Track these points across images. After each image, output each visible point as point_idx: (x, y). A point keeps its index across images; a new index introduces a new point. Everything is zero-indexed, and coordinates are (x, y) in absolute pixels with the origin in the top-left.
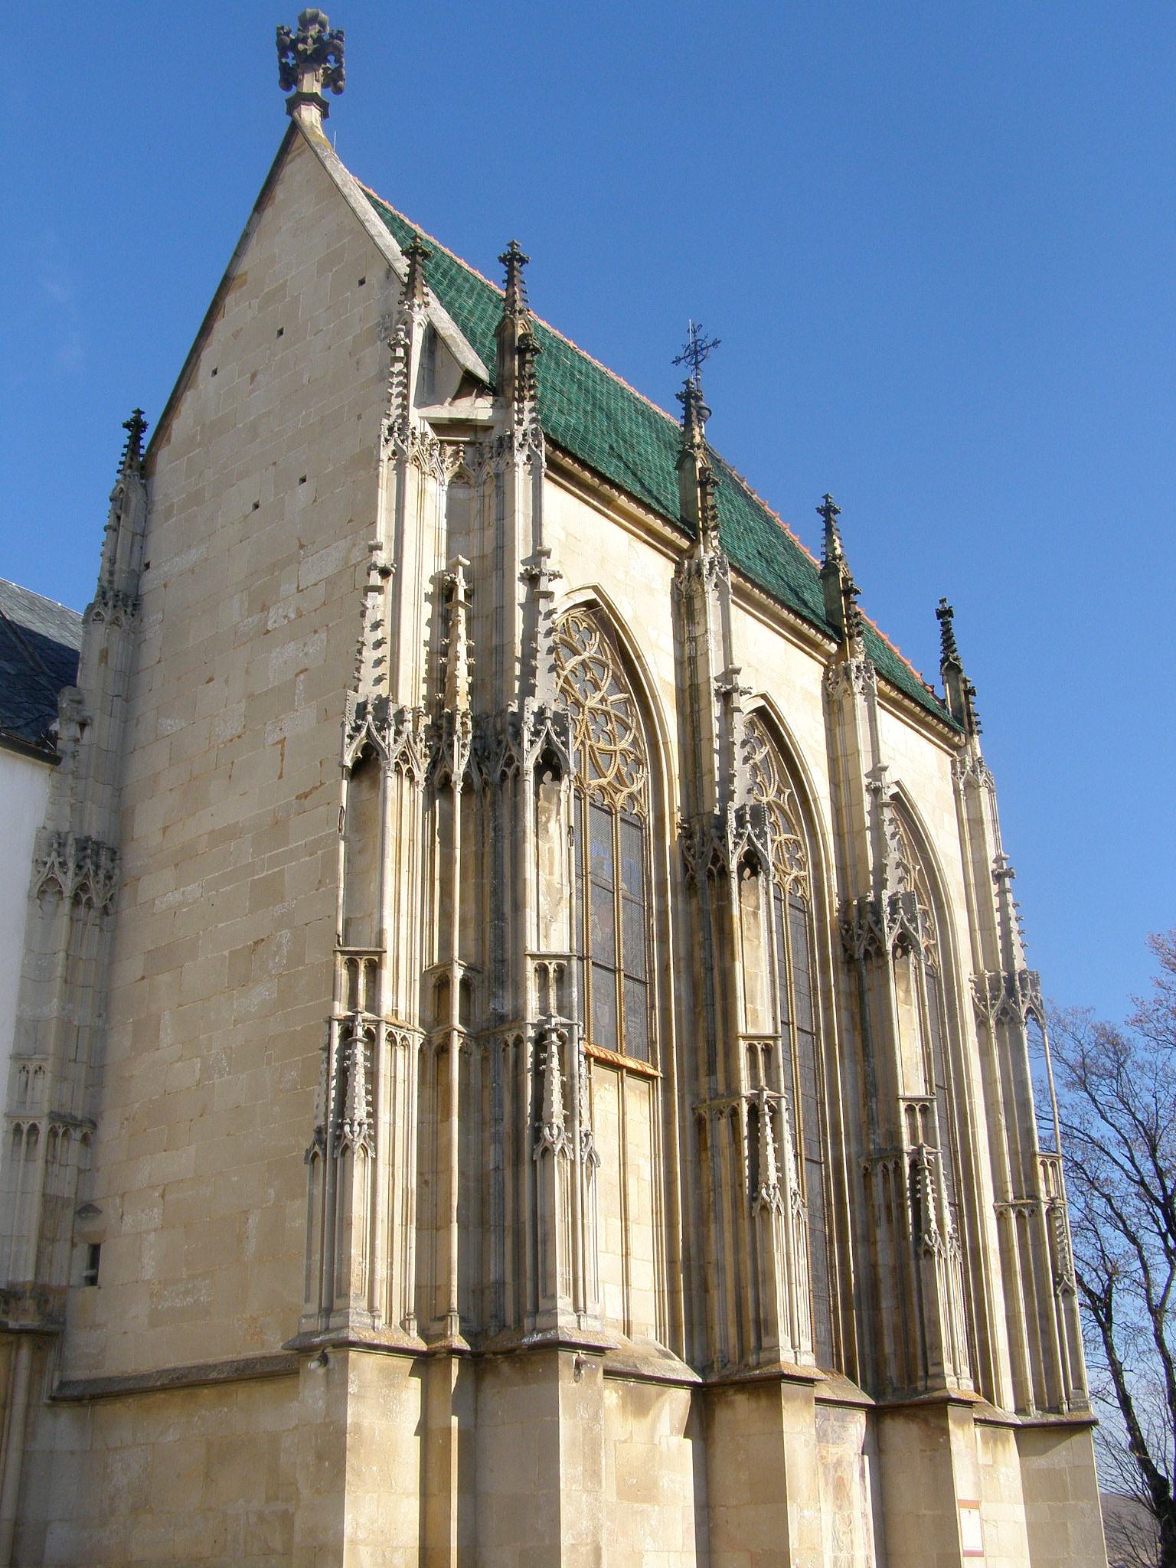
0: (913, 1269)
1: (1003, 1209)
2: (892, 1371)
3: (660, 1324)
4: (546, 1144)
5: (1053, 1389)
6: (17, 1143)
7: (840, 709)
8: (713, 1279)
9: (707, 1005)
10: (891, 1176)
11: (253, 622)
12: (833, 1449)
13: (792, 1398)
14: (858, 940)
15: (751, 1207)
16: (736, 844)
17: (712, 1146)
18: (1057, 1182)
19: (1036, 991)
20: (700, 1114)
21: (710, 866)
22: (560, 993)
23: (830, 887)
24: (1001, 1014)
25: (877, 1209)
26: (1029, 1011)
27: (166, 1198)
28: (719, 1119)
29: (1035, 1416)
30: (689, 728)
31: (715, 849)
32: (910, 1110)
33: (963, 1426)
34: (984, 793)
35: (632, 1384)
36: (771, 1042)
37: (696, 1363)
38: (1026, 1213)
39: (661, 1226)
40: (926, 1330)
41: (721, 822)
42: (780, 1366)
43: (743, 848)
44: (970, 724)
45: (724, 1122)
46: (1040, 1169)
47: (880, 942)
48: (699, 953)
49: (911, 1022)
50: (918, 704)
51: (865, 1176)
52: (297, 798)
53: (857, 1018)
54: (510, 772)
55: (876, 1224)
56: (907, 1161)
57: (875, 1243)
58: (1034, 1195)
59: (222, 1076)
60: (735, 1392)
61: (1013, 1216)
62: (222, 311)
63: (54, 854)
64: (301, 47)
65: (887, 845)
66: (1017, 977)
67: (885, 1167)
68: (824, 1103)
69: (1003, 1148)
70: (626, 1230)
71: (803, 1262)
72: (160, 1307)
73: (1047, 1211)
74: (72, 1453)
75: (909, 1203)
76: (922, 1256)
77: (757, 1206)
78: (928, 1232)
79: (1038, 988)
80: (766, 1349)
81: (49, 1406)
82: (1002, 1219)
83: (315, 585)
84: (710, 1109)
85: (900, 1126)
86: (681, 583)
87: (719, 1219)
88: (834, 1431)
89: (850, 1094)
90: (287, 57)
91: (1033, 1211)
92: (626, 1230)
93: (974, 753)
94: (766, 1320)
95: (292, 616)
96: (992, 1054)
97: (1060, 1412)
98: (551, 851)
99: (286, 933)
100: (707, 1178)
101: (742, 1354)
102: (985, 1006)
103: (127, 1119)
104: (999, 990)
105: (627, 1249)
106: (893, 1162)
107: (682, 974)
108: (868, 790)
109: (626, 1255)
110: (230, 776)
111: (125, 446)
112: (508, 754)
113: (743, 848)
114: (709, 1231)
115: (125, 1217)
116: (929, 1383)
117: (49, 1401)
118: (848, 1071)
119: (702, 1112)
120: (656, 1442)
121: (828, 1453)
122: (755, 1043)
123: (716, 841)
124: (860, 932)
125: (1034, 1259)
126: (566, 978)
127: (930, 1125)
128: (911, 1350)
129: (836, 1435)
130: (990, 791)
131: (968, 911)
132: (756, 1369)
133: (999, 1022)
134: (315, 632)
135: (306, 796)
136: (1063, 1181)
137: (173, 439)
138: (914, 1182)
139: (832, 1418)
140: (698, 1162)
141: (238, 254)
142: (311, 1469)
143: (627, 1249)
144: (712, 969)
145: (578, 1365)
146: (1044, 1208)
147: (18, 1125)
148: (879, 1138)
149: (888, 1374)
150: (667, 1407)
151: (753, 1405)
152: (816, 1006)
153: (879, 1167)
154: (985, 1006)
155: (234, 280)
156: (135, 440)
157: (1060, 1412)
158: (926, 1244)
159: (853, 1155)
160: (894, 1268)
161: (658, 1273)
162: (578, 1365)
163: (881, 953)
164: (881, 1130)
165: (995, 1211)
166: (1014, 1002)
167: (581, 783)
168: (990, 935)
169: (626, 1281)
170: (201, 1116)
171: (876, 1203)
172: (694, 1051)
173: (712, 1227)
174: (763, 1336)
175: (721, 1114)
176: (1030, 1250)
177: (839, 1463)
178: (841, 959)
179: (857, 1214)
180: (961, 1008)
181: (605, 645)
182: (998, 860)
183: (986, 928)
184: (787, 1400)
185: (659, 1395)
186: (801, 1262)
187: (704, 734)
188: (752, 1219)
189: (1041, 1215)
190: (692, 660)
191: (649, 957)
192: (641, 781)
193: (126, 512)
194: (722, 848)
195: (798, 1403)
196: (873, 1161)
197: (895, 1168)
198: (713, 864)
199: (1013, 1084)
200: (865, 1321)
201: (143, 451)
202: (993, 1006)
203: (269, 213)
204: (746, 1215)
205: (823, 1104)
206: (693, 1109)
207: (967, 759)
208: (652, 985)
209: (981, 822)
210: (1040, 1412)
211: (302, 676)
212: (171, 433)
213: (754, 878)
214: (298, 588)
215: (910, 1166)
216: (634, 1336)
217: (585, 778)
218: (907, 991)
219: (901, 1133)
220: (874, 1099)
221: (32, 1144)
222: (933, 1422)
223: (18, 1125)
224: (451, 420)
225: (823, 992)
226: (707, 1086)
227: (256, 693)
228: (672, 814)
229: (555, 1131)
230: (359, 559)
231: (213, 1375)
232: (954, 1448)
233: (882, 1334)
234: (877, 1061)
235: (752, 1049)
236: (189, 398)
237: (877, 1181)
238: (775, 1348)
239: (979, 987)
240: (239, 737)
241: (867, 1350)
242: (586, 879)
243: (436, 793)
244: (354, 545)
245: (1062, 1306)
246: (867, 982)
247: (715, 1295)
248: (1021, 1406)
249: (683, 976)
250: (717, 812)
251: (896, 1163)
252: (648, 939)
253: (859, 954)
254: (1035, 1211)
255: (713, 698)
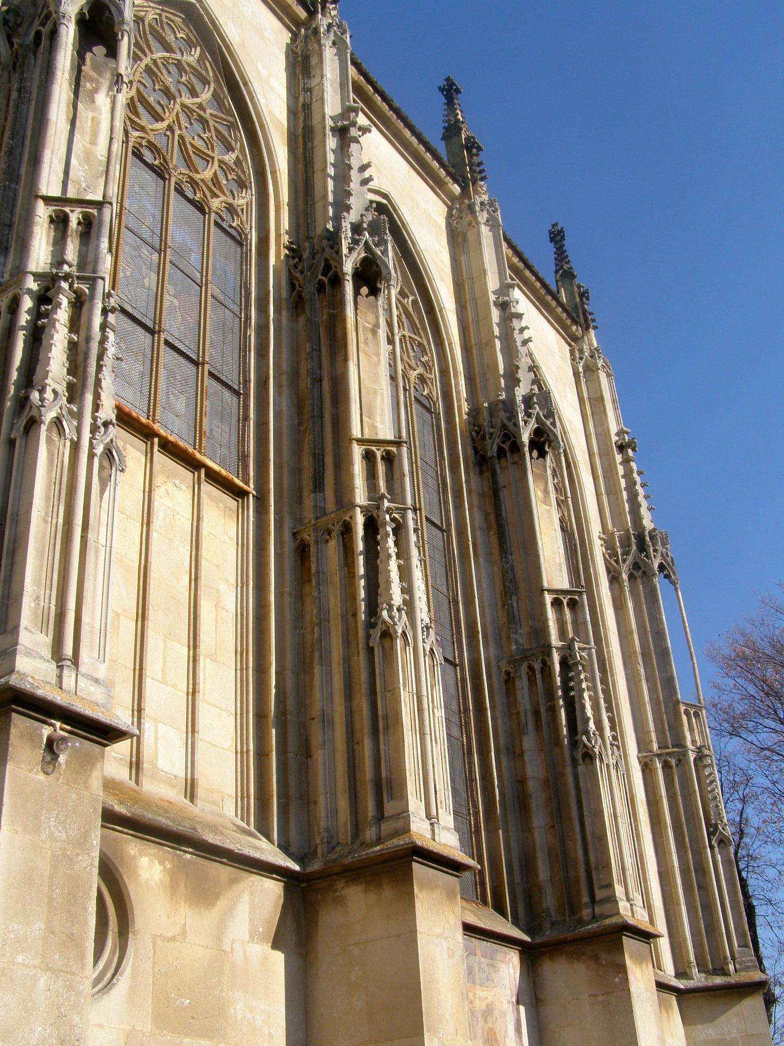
0: (570, 778)
1: (647, 760)
2: (549, 901)
3: (243, 795)
4: (34, 413)
5: (716, 948)
7: (465, 239)
8: (317, 734)
9: (313, 417)
10: (539, 676)
12: (481, 992)
13: (430, 886)
14: (490, 438)
15: (368, 637)
16: (351, 250)
17: (318, 572)
18: (702, 732)
19: (666, 549)
20: (302, 541)
21: (320, 277)
22: (84, 248)
23: (458, 393)
24: (634, 568)
25: (522, 717)
26: (662, 567)
28: (327, 541)
29: (698, 979)
30: (301, 166)
31: (326, 260)
32: (557, 603)
33: (640, 964)
34: (602, 376)
35: (188, 856)
36: (394, 449)
37: (292, 849)
38: (673, 762)
39: (247, 668)
40: (590, 847)
41: (333, 238)
42: (410, 837)
43: (359, 254)
44: (586, 319)
45: (333, 547)
46: (684, 718)
47: (514, 437)
48: (305, 366)
49: (552, 522)
50: (539, 279)
51: (507, 682)
53: (492, 518)
54: (45, 31)
55: (522, 732)
56: (556, 657)
57: (522, 755)
58: (679, 743)
60: (347, 882)
61: (659, 766)
65: (518, 351)
66: (648, 538)
67: (531, 668)
68: (458, 602)
69: (644, 699)
70: (194, 660)
71: (440, 713)
73: (695, 760)
75: (561, 702)
76: (581, 761)
77: (376, 633)
78: (586, 732)
79: (668, 546)
80: (391, 817)
82: (647, 771)
84: (316, 530)
85: (546, 620)
86: (297, 47)
87: (326, 659)
88: (481, 970)
89: (486, 595)
91: (679, 761)
92: (194, 660)
93: (590, 344)
94: (390, 781)
96: (627, 607)
97: (726, 973)
98: (96, 122)
100: (311, 612)
101: (357, 829)
102: (617, 561)
104: (629, 545)
105: (194, 684)
106: (539, 660)
107: (284, 388)
108: (495, 304)
109: (193, 693)
112: (45, 12)
113: (359, 254)
114: (312, 679)
116: (598, 910)
118: (483, 570)
119: (305, 536)
120: (227, 947)
121: (475, 995)
122: (374, 448)
123: (328, 250)
124: (492, 430)
125: (684, 810)
126: (94, 231)
127: (580, 621)
128: (572, 874)
129: (484, 976)
130: (608, 375)
131: (594, 479)
132: (376, 846)
133: (631, 577)
136: (708, 731)
138: (566, 680)
139: (478, 952)
140: (300, 597)
143: (194, 684)
144: (321, 381)
145: (51, 746)
146: (692, 756)
148: (521, 637)
149: (544, 905)
150: (245, 899)
151: (373, 897)
152: (446, 503)
153: (524, 669)
154: (617, 561)
157: (726, 973)
158: (585, 746)
159: (492, 658)
160: (546, 781)
161: (241, 728)
162: (51, 746)
163: (516, 447)
164: (524, 630)
165: (640, 762)
166: (646, 556)
167: (165, 160)
168: (617, 499)
169: (192, 727)
171: (522, 709)
172: (297, 472)
173: (317, 670)
174: (385, 801)
175: (329, 534)
176: (680, 801)
177: (489, 1011)
178: (472, 459)
179: (499, 722)
180: (593, 561)
181: (208, 64)
182: (620, 433)
183: (612, 491)
184: (422, 887)
185: (233, 881)
186: (437, 714)
187: (317, 166)
188: (370, 650)
189: (689, 763)
190: (307, 107)
191: (244, 368)
192: (245, 199)
194: (335, 255)
195: (436, 894)
196: (515, 662)
197: (542, 668)
198: (325, 274)
199: (650, 635)
200: (514, 844)
202: (624, 561)
204: (362, 644)
205: (456, 602)
206: (294, 534)
207: (585, 347)
208: (247, 396)
209: (602, 399)
210: (703, 975)
213: (372, 298)
215: (561, 663)
216: (199, 802)
217: (172, 159)
218: (546, 491)
219: (548, 626)
220: (514, 598)
222: (604, 958)
225: (453, 491)
226: (312, 504)
228: (278, 236)
229: (49, 395)
232: (633, 989)
233: (534, 858)
234: (516, 558)
235: (369, 457)
237: (522, 685)
238: (403, 815)
239: (609, 544)
241: (517, 878)
242: (165, 256)
245: (719, 857)
246: (502, 479)
247: (319, 756)
248: (681, 970)
249: (285, 391)
250: (330, 226)
251: (544, 662)
252: (244, 349)
253: (492, 451)
254: (682, 760)
255: (329, 133)
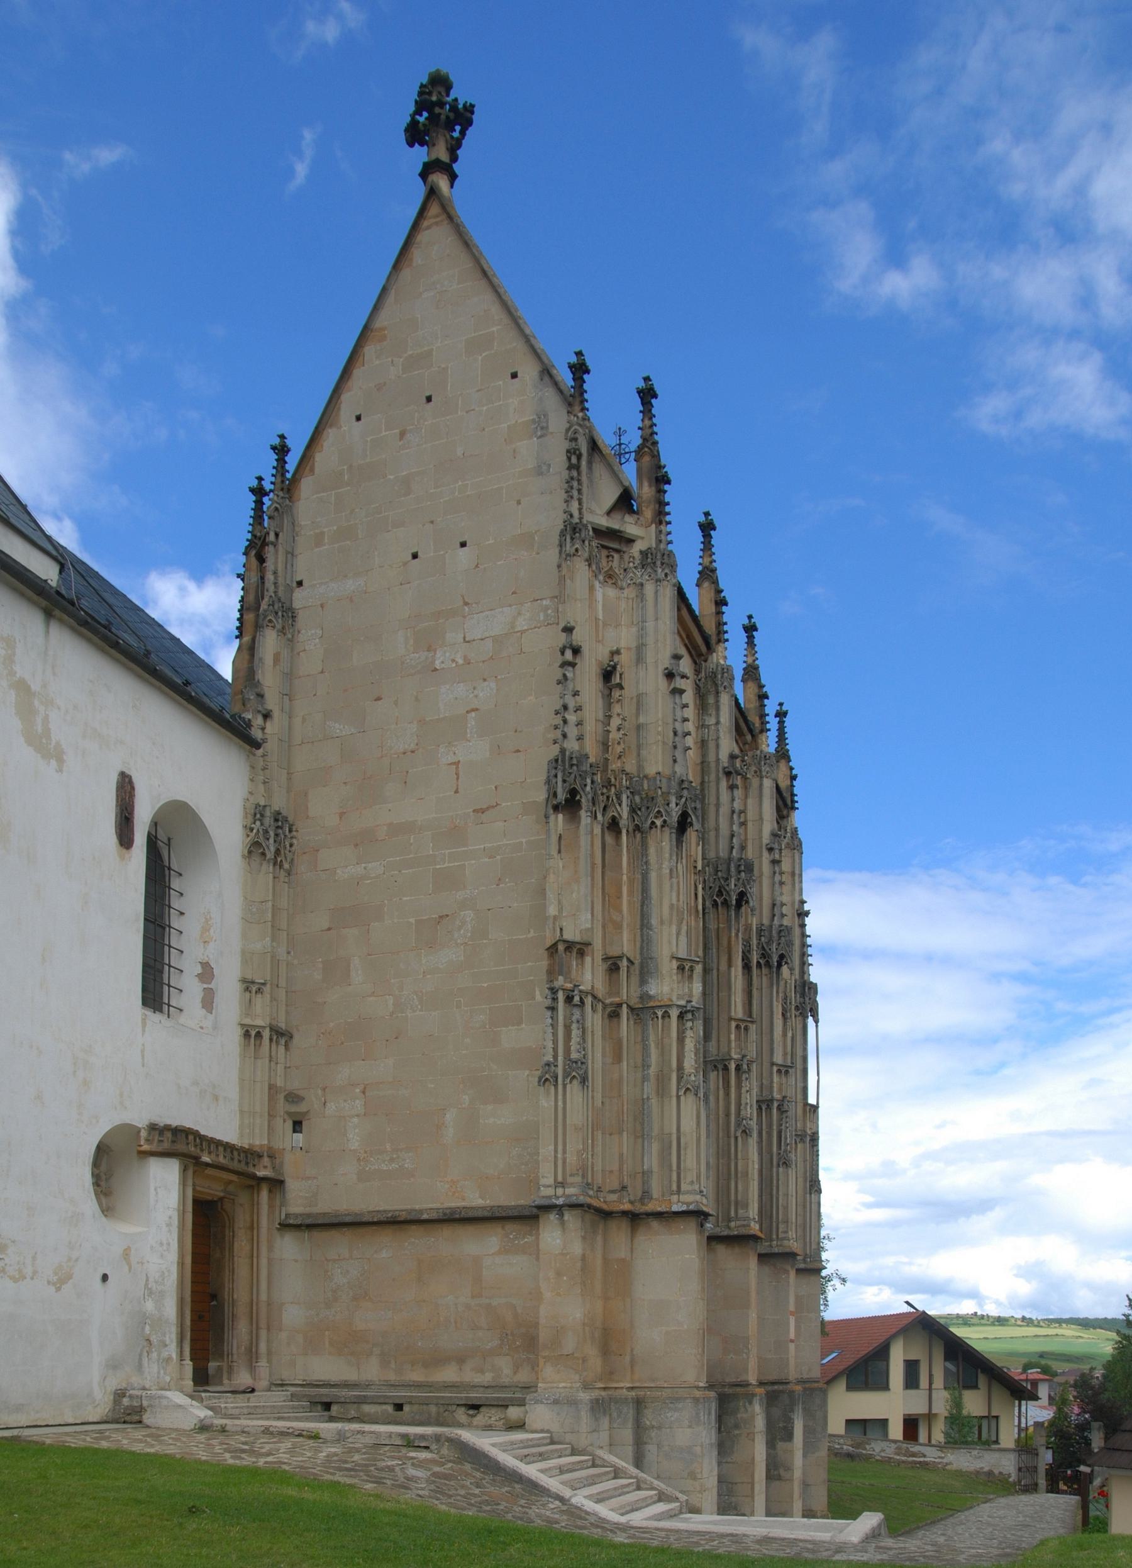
6: (246, 1045)
11: (419, 657)
21: (715, 897)
27: (367, 1094)
52: (474, 811)
59: (414, 1011)
62: (361, 358)
63: (258, 823)
64: (437, 110)
72: (367, 1169)
74: (296, 1261)
81: (278, 1229)
83: (482, 639)
90: (421, 115)
95: (461, 661)
99: (469, 915)
103: (322, 1033)
110: (405, 782)
111: (274, 468)
115: (328, 1104)
117: (278, 1226)
134: (485, 680)
135: (483, 811)
137: (317, 470)
141: (376, 308)
142: (552, 1280)
147: (247, 1031)
155: (372, 331)
156: (281, 462)
170: (396, 1038)
193: (282, 530)
201: (289, 476)
203: (406, 274)
211: (473, 714)
212: (314, 464)
214: (464, 638)
221: (258, 1046)
223: (247, 1031)
224: (608, 528)
227: (427, 719)
230: (525, 628)
231: (425, 1216)
236: (330, 436)
240: (413, 752)
243: (606, 830)
244: (519, 614)
